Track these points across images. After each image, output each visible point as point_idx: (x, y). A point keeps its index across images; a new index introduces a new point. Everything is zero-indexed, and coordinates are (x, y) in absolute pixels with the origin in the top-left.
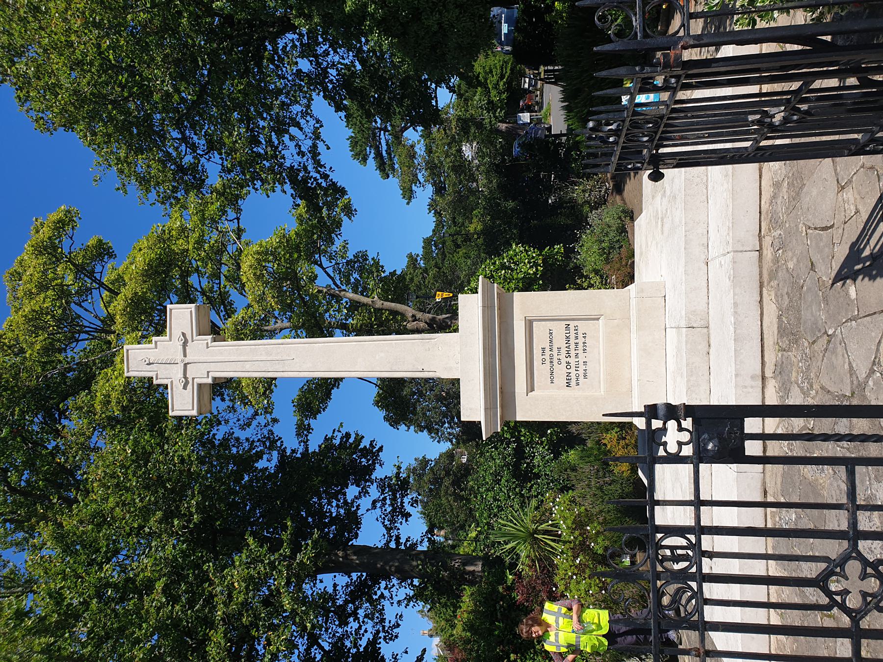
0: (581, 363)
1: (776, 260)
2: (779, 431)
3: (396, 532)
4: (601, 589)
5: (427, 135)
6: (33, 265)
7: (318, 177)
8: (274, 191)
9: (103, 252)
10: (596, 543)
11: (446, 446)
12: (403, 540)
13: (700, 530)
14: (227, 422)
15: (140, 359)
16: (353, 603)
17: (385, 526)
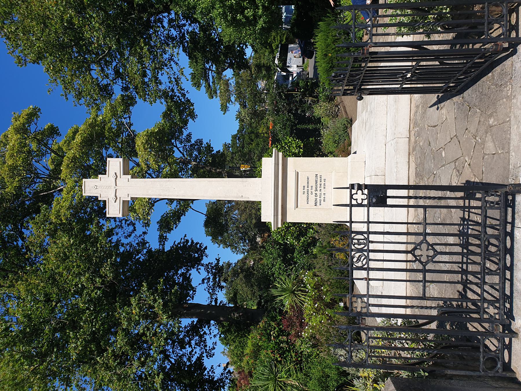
0: (322, 194)
1: (416, 142)
2: (414, 222)
3: (215, 296)
4: (328, 320)
5: (236, 75)
6: (14, 139)
7: (180, 96)
8: (155, 102)
9: (53, 131)
10: (326, 295)
11: (241, 256)
12: (219, 302)
13: (369, 233)
14: (117, 234)
15: (91, 187)
16: (189, 337)
17: (210, 293)
